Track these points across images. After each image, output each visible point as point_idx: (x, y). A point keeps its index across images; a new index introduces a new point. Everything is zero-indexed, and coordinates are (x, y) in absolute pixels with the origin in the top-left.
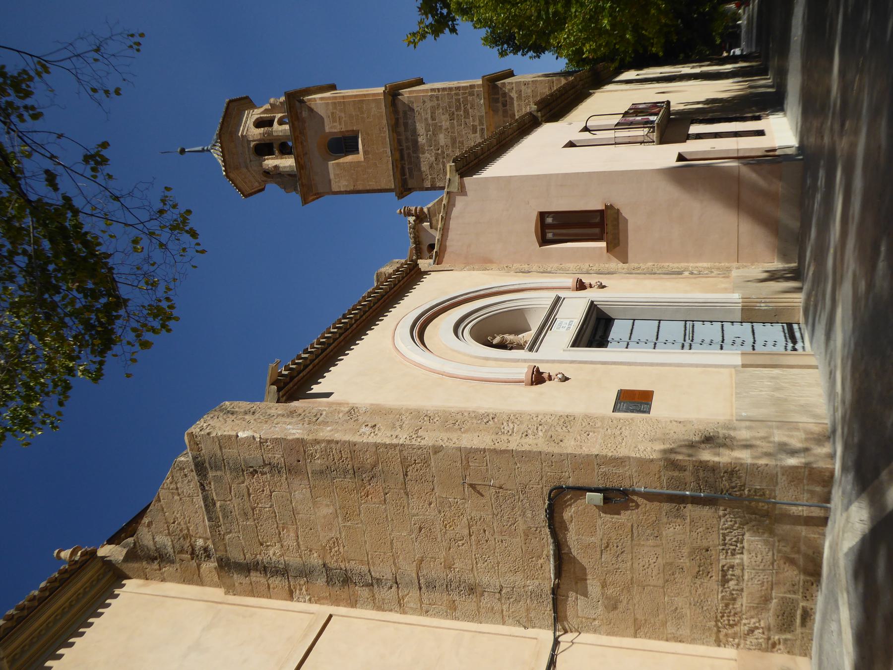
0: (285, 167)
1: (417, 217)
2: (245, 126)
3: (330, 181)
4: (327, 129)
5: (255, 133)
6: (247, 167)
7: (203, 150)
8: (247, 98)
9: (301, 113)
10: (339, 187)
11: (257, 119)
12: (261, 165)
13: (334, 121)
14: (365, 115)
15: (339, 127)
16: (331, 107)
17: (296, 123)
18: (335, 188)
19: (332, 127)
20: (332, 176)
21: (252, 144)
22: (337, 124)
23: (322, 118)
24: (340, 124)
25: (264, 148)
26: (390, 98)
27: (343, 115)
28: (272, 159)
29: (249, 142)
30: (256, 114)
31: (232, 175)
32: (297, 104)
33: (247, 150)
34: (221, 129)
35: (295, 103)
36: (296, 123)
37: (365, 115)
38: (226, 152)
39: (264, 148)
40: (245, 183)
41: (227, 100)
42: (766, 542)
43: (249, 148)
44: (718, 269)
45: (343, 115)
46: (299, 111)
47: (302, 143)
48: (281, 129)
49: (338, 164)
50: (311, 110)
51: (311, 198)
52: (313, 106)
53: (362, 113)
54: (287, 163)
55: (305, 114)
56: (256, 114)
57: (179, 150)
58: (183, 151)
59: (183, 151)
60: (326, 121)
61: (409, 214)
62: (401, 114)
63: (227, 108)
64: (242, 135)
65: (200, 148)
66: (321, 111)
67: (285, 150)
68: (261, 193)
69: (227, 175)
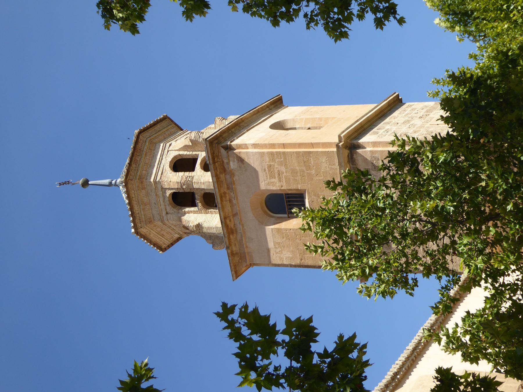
0: (210, 228)
2: (159, 168)
3: (268, 250)
4: (263, 186)
5: (173, 180)
6: (162, 221)
7: (110, 184)
8: (165, 118)
9: (228, 163)
10: (281, 259)
11: (175, 157)
12: (180, 220)
13: (272, 176)
14: (313, 172)
15: (278, 184)
17: (222, 176)
18: (275, 259)
19: (269, 184)
20: (271, 245)
21: (168, 193)
22: (276, 180)
23: (255, 170)
24: (280, 181)
25: (184, 198)
26: (347, 152)
27: (283, 169)
28: (195, 212)
29: (164, 190)
30: (176, 146)
31: (143, 231)
32: (223, 151)
33: (161, 199)
36: (222, 176)
37: (313, 172)
38: (134, 203)
39: (184, 198)
40: (163, 236)
41: (137, 131)
43: (164, 197)
46: (225, 161)
47: (230, 201)
48: (202, 179)
49: (279, 230)
50: (241, 160)
51: (244, 269)
52: (243, 156)
53: (309, 168)
54: (211, 220)
55: (233, 165)
56: (176, 146)
57: (81, 182)
58: (86, 184)
59: (86, 184)
60: (261, 175)
63: (136, 142)
64: (155, 182)
65: (106, 181)
67: (209, 201)
68: (180, 241)
69: (137, 232)
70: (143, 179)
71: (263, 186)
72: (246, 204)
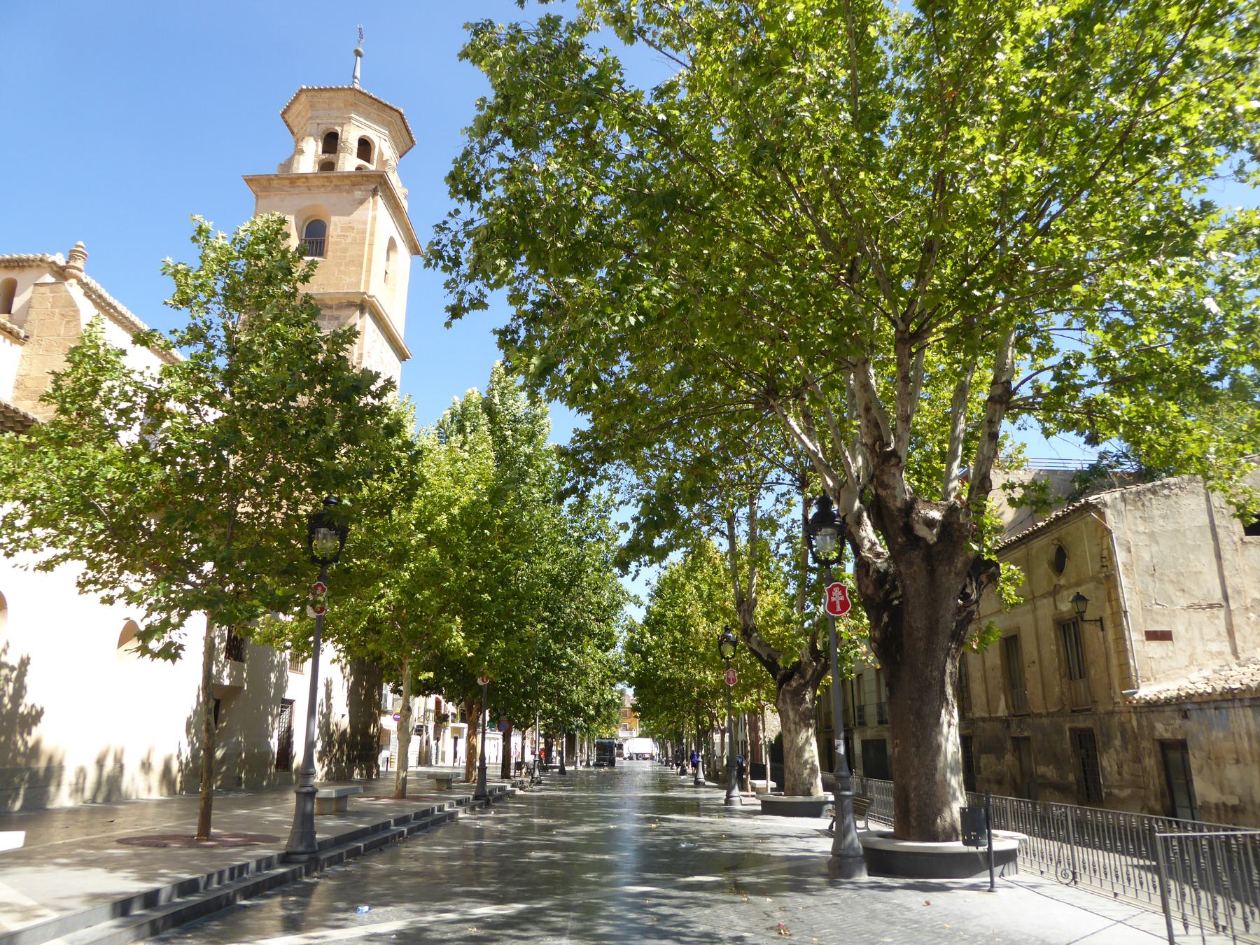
1: (63, 269)
4: (334, 219)
5: (351, 135)
7: (355, 77)
8: (413, 142)
13: (343, 229)
16: (361, 227)
17: (348, 182)
19: (336, 226)
21: (338, 129)
22: (339, 232)
23: (349, 214)
26: (358, 301)
27: (349, 240)
29: (342, 125)
31: (303, 97)
32: (373, 186)
34: (364, 94)
35: (379, 184)
39: (331, 142)
42: (1101, 755)
43: (335, 124)
44: (427, 742)
45: (349, 240)
48: (349, 162)
50: (362, 202)
52: (365, 204)
55: (358, 194)
58: (358, 53)
61: (72, 256)
62: (336, 313)
65: (358, 74)
66: (359, 214)
67: (327, 166)
70: (355, 107)
71: (334, 219)
72: (319, 201)
